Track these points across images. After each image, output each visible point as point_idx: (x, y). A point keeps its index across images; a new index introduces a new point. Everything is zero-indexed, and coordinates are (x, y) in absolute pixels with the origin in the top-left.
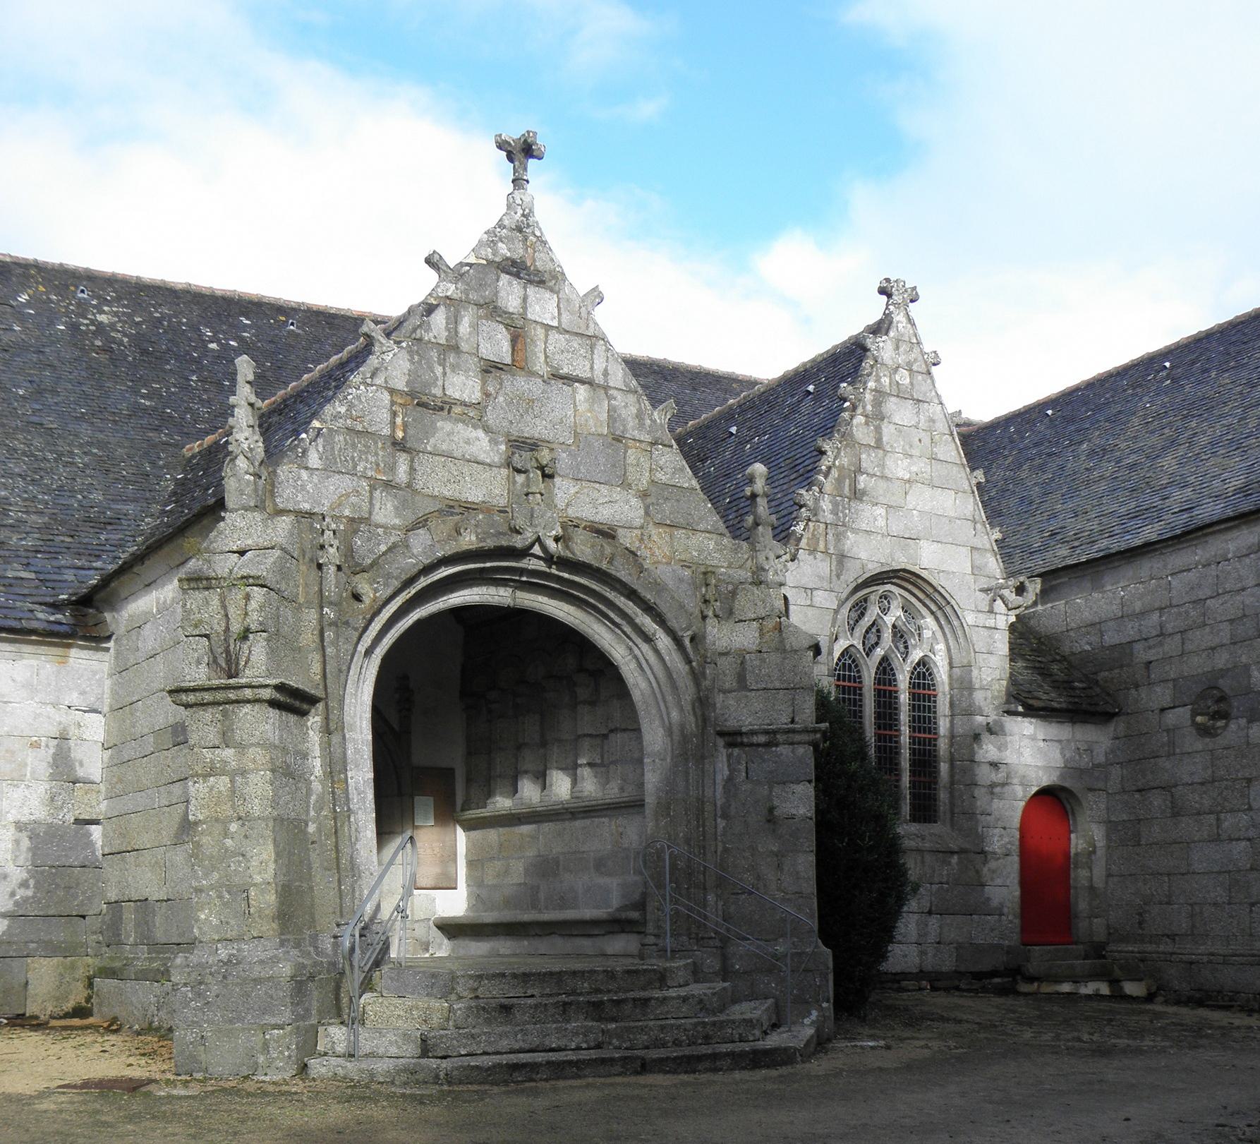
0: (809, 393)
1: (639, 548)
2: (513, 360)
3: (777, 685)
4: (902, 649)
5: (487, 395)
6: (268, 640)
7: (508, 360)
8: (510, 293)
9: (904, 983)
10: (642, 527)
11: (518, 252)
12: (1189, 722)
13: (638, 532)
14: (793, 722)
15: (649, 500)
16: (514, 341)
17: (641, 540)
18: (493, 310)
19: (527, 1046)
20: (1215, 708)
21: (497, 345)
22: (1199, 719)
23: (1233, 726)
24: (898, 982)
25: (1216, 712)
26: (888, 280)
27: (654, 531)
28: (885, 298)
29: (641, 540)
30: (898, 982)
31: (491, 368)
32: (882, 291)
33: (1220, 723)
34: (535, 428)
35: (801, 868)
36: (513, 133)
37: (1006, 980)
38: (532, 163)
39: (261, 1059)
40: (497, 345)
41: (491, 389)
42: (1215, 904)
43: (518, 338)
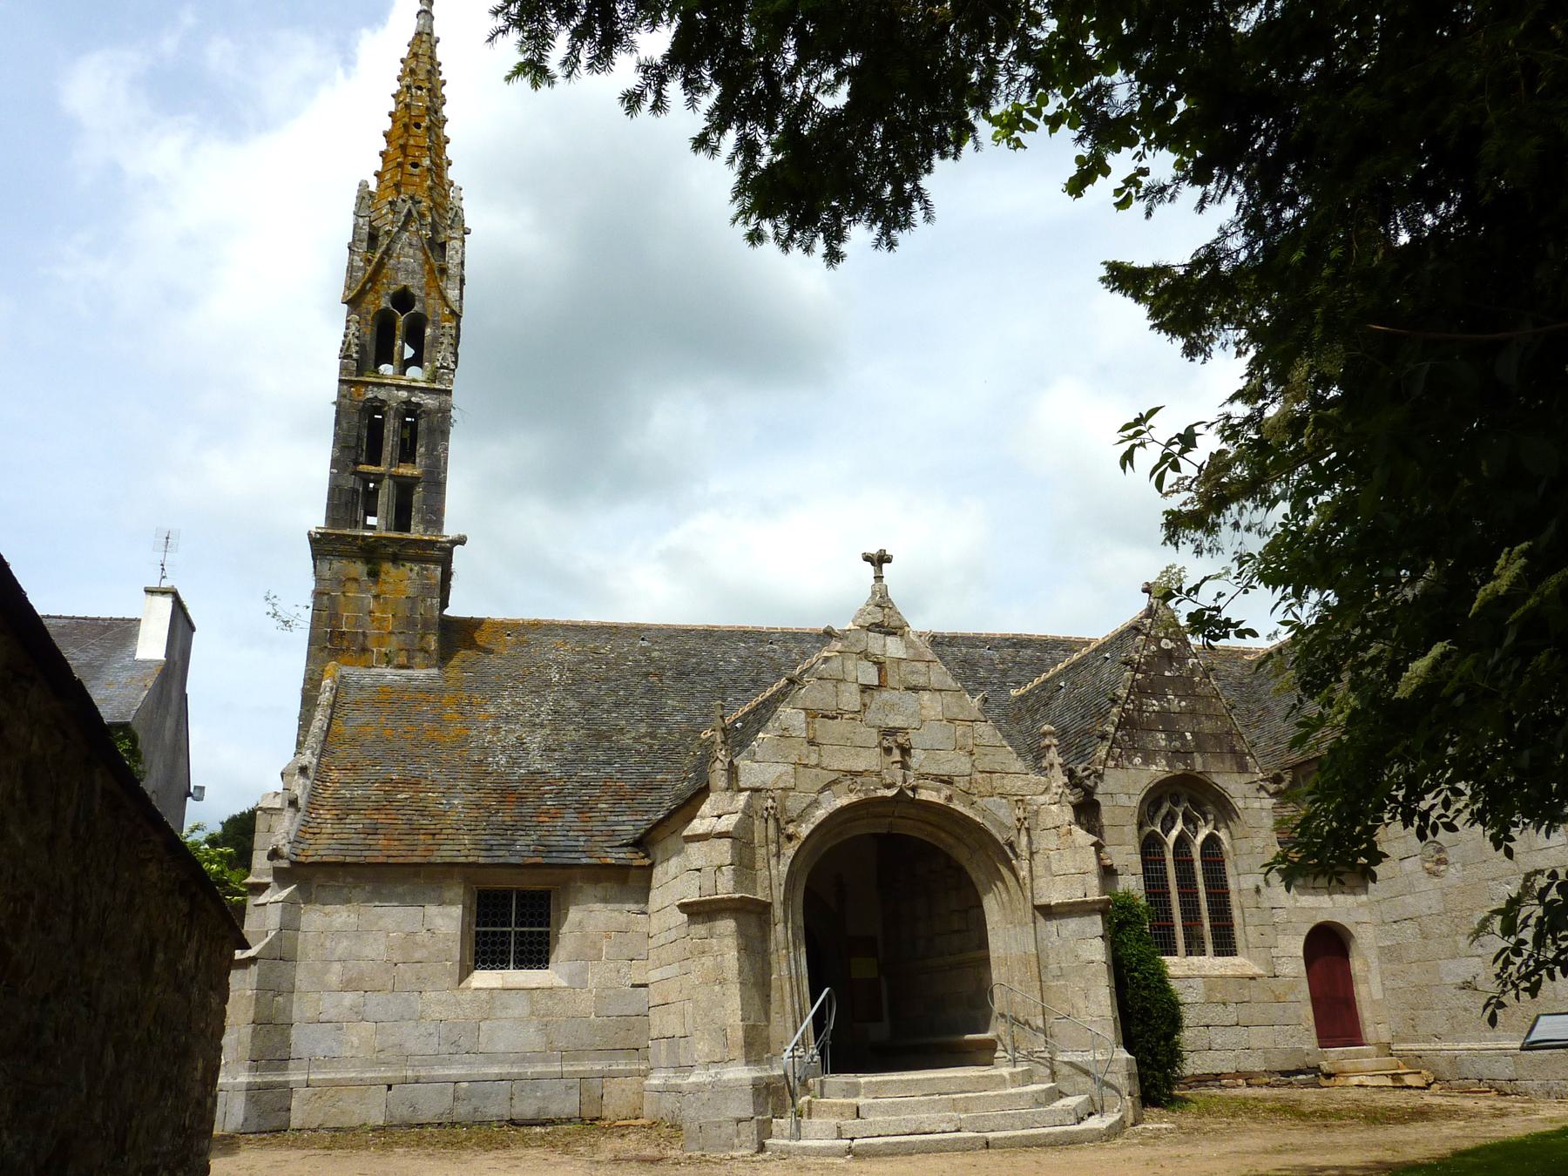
0: (1107, 659)
1: (969, 788)
2: (880, 682)
3: (1073, 871)
4: (1193, 830)
5: (865, 705)
6: (733, 870)
7: (876, 683)
8: (875, 642)
9: (1224, 1082)
10: (970, 775)
11: (879, 618)
12: (1421, 868)
13: (968, 778)
14: (1085, 896)
15: (974, 757)
16: (880, 671)
17: (971, 783)
18: (865, 655)
19: (908, 1131)
20: (1437, 856)
21: (870, 675)
22: (1427, 865)
23: (1452, 870)
24: (1220, 1080)
25: (1439, 860)
26: (1147, 583)
27: (978, 776)
28: (1147, 595)
29: (971, 783)
30: (1220, 1080)
31: (865, 689)
32: (1144, 591)
33: (1442, 867)
34: (896, 721)
35: (1101, 998)
36: (873, 550)
37: (1310, 1076)
38: (885, 566)
39: (736, 1141)
40: (870, 675)
41: (867, 701)
42: (440, 1124)
43: (880, 665)
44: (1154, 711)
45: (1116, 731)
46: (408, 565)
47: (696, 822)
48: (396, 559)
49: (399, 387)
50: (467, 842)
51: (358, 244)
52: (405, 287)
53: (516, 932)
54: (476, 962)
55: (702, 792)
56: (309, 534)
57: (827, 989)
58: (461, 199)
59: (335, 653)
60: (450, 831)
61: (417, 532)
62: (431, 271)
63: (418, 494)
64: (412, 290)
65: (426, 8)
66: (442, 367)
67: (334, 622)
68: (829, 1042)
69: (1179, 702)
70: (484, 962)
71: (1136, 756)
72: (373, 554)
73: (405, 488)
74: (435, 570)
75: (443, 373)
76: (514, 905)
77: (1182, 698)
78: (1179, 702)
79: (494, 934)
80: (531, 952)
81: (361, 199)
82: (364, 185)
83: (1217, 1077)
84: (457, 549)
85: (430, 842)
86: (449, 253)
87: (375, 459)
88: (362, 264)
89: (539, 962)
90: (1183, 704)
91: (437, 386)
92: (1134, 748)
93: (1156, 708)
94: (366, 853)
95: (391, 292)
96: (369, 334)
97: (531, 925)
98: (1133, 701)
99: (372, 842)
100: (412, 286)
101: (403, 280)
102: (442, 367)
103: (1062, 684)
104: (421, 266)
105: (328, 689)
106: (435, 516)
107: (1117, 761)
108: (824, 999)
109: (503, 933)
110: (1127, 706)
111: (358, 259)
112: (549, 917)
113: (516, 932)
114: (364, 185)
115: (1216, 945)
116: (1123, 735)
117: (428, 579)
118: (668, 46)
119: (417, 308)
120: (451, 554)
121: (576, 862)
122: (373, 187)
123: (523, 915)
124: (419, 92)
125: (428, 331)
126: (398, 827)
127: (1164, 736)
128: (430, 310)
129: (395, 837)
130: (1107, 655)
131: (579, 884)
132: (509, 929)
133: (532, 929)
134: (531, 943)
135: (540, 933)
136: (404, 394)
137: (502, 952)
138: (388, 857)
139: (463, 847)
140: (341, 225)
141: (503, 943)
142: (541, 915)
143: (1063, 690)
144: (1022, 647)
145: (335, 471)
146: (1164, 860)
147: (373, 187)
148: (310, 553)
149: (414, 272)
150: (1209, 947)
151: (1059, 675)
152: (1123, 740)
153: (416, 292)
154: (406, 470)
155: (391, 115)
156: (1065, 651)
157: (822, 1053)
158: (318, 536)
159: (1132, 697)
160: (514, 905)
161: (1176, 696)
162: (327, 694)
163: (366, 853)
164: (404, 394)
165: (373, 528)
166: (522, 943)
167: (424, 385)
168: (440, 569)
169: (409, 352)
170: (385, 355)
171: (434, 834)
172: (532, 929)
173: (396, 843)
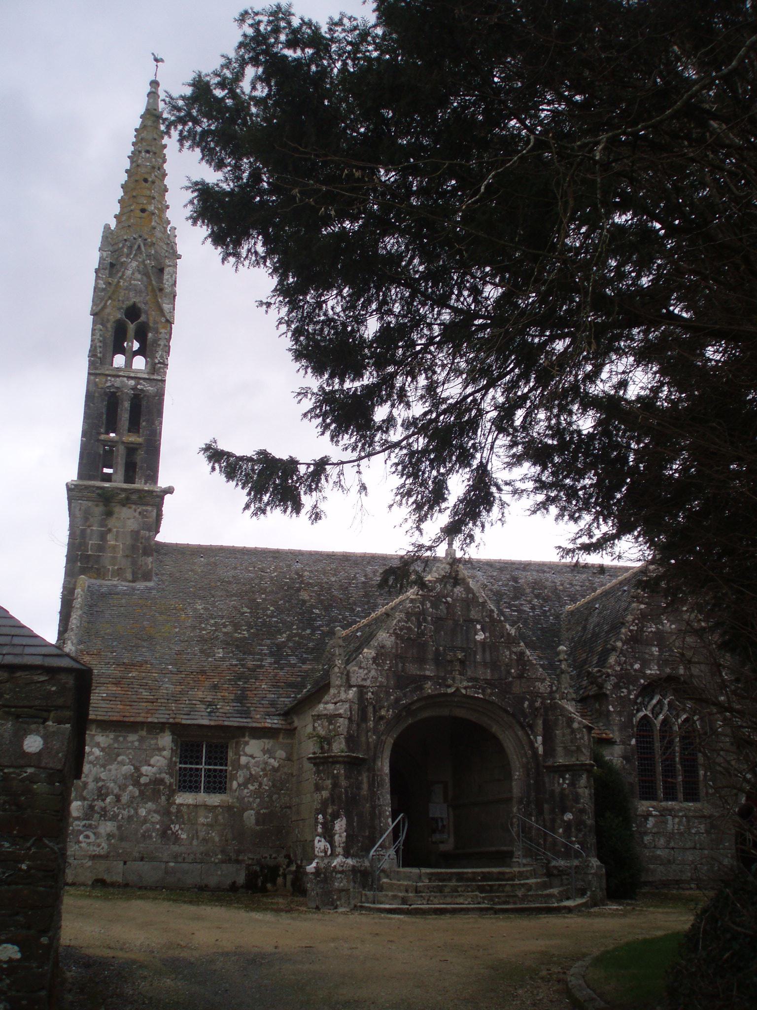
44: (652, 631)
45: (623, 646)
46: (134, 507)
47: (321, 706)
48: (126, 502)
49: (129, 378)
50: (174, 708)
51: (102, 271)
52: (134, 304)
53: (205, 769)
54: (180, 787)
55: (326, 687)
56: (67, 484)
57: (402, 815)
58: (176, 236)
59: (83, 571)
60: (163, 701)
61: (139, 485)
62: (153, 290)
63: (141, 453)
64: (139, 305)
65: (153, 90)
66: (160, 363)
67: (83, 548)
68: (402, 847)
69: (671, 625)
70: (185, 787)
71: (636, 663)
72: (107, 499)
73: (131, 450)
74: (152, 511)
75: (160, 367)
76: (204, 751)
77: (672, 623)
78: (671, 625)
79: (191, 769)
80: (215, 782)
81: (105, 238)
82: (107, 227)
83: (678, 882)
84: (167, 497)
85: (151, 708)
86: (166, 277)
87: (112, 426)
88: (104, 286)
89: (220, 788)
90: (673, 626)
91: (155, 377)
92: (635, 657)
93: (653, 630)
94: (110, 714)
95: (124, 306)
96: (110, 335)
97: (215, 764)
98: (637, 624)
99: (113, 706)
100: (140, 302)
101: (134, 299)
102: (160, 363)
103: (597, 606)
104: (146, 288)
105: (79, 596)
106: (152, 475)
107: (622, 666)
108: (399, 821)
109: (197, 769)
110: (632, 628)
111: (102, 282)
112: (227, 760)
113: (205, 769)
114: (107, 227)
115: (665, 794)
116: (628, 648)
117: (147, 517)
118: (277, 457)
119: (143, 318)
120: (163, 499)
121: (246, 725)
122: (113, 227)
123: (210, 758)
124: (148, 155)
125: (150, 335)
126: (129, 696)
127: (657, 649)
128: (151, 319)
129: (128, 703)
130: (625, 588)
131: (247, 739)
132: (201, 767)
133: (216, 767)
134: (215, 777)
135: (221, 771)
136: (132, 383)
137: (196, 782)
138: (124, 717)
139: (171, 712)
140: (92, 258)
141: (197, 776)
142: (221, 758)
143: (597, 611)
144: (578, 573)
145: (84, 439)
146: (653, 735)
147: (113, 227)
148: (66, 496)
149: (141, 292)
150: (681, 796)
151: (595, 600)
152: (628, 651)
153: (142, 306)
154: (133, 438)
155: (127, 171)
156: (611, 576)
157: (397, 852)
158: (73, 487)
159: (637, 621)
160: (204, 751)
161: (668, 621)
162: (79, 600)
163: (110, 714)
164: (132, 383)
165: (108, 478)
166: (209, 776)
167: (146, 376)
168: (155, 511)
169: (136, 346)
170: (119, 349)
171: (153, 702)
172: (216, 767)
173: (128, 707)
